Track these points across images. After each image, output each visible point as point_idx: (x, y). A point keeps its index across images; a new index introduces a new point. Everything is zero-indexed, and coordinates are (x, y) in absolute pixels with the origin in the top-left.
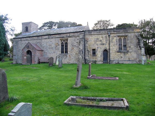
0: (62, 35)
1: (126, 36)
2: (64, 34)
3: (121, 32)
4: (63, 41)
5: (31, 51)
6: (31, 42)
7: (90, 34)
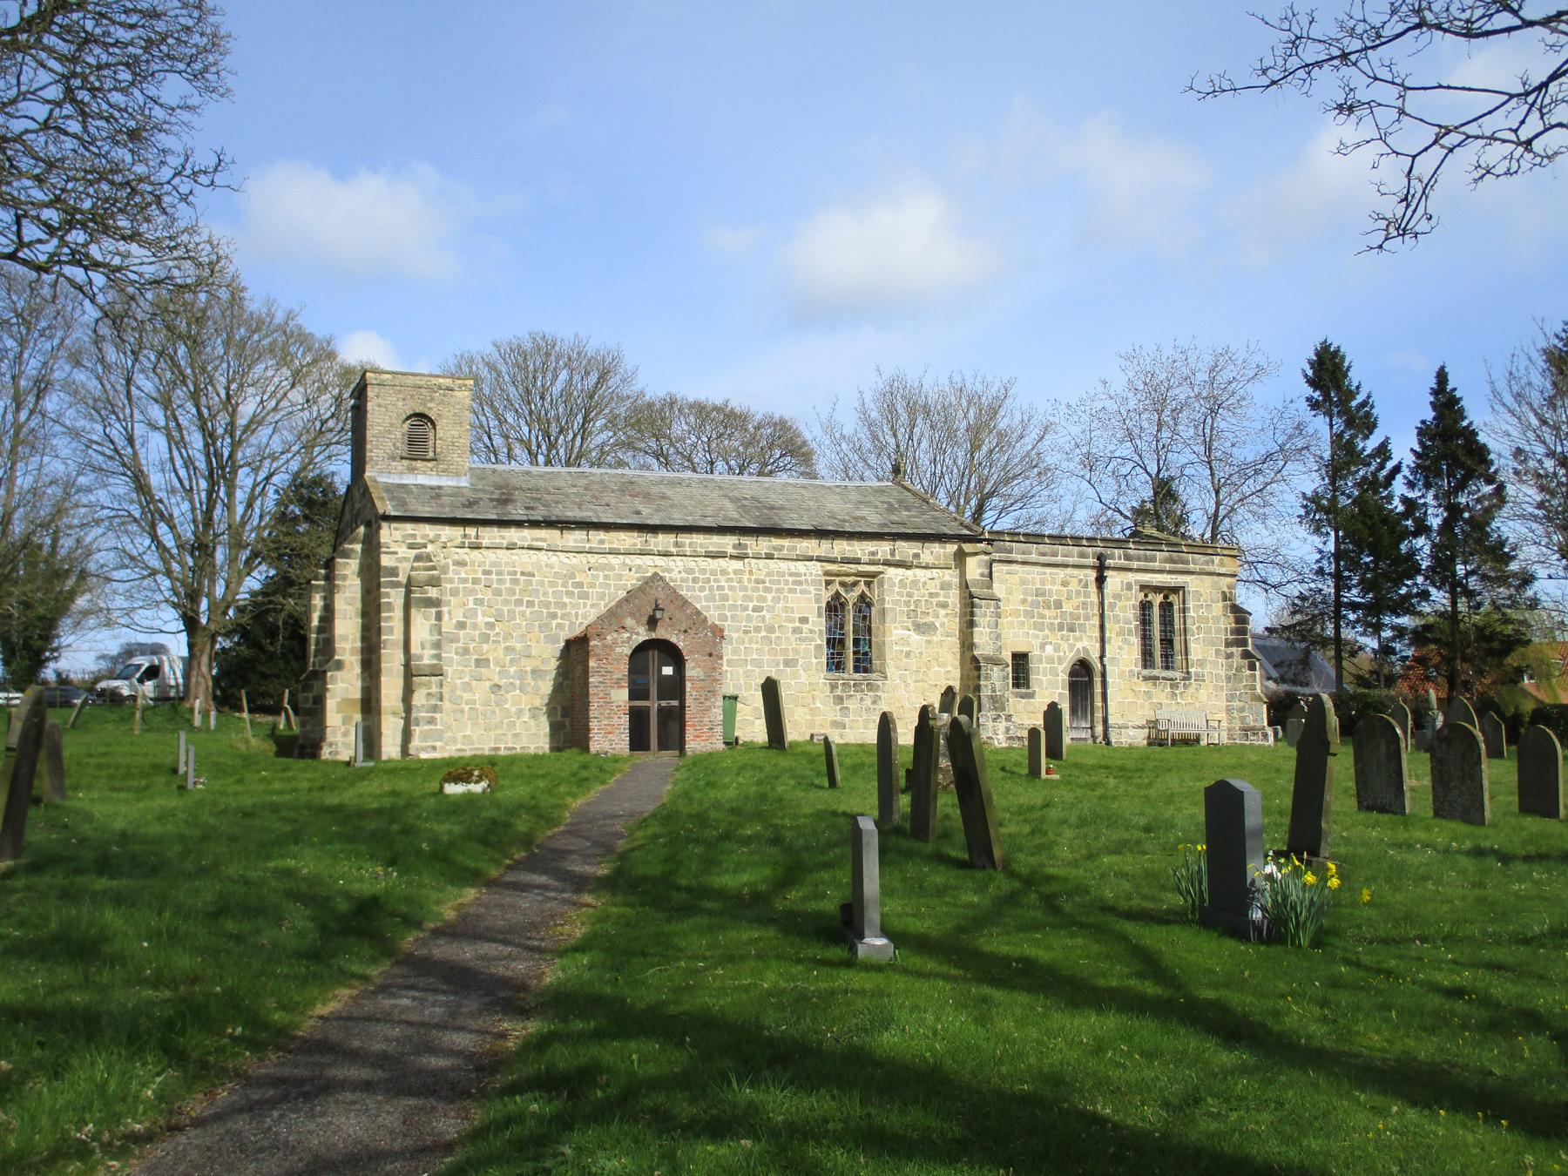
0: (602, 535)
1: (1175, 590)
2: (613, 535)
3: (1156, 565)
4: (843, 584)
5: (681, 645)
6: (676, 570)
7: (1180, 566)
